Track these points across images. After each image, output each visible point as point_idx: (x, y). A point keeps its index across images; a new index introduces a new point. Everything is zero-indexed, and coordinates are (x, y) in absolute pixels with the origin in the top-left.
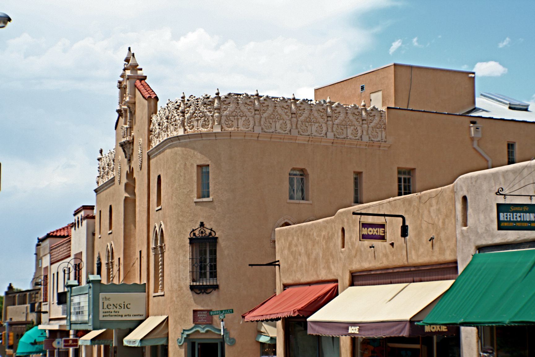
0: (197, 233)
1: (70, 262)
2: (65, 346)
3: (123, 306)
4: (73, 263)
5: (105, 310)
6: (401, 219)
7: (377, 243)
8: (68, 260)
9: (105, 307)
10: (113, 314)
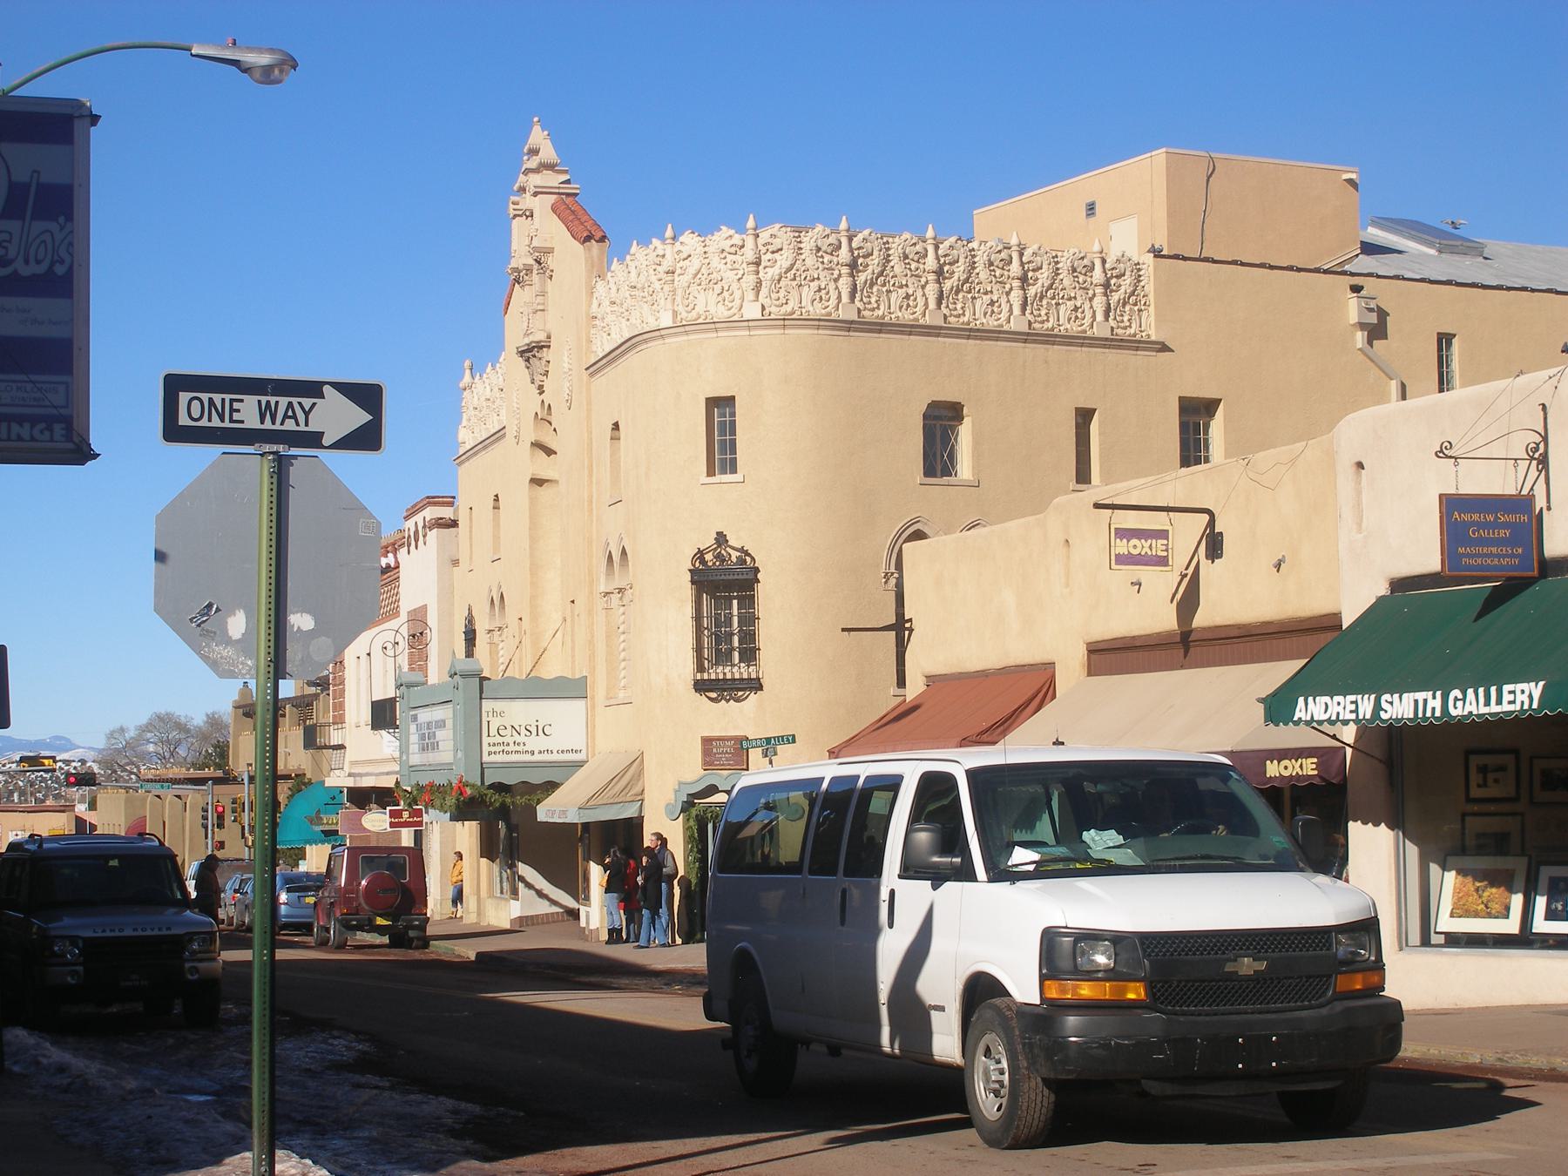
0: (709, 557)
1: (400, 624)
2: (392, 825)
3: (534, 730)
4: (404, 631)
5: (492, 740)
6: (1206, 517)
7: (1145, 573)
8: (394, 624)
9: (493, 731)
10: (512, 748)
